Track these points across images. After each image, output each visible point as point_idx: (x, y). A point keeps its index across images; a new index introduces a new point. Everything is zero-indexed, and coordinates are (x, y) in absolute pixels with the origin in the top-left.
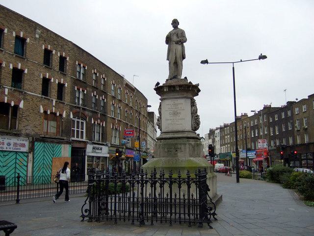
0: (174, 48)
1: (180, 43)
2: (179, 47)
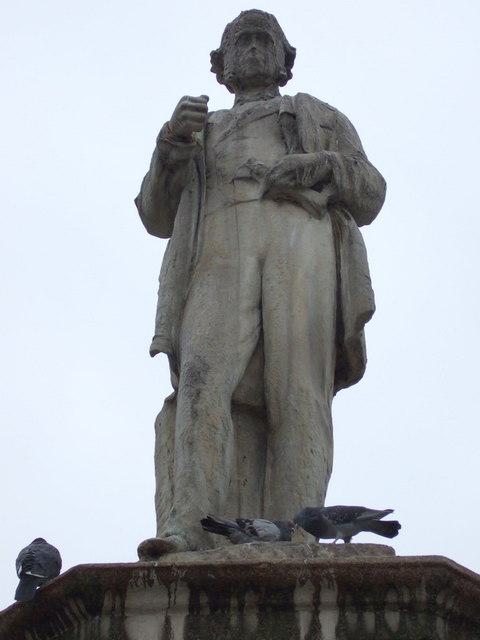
1: (319, 198)
2: (307, 236)
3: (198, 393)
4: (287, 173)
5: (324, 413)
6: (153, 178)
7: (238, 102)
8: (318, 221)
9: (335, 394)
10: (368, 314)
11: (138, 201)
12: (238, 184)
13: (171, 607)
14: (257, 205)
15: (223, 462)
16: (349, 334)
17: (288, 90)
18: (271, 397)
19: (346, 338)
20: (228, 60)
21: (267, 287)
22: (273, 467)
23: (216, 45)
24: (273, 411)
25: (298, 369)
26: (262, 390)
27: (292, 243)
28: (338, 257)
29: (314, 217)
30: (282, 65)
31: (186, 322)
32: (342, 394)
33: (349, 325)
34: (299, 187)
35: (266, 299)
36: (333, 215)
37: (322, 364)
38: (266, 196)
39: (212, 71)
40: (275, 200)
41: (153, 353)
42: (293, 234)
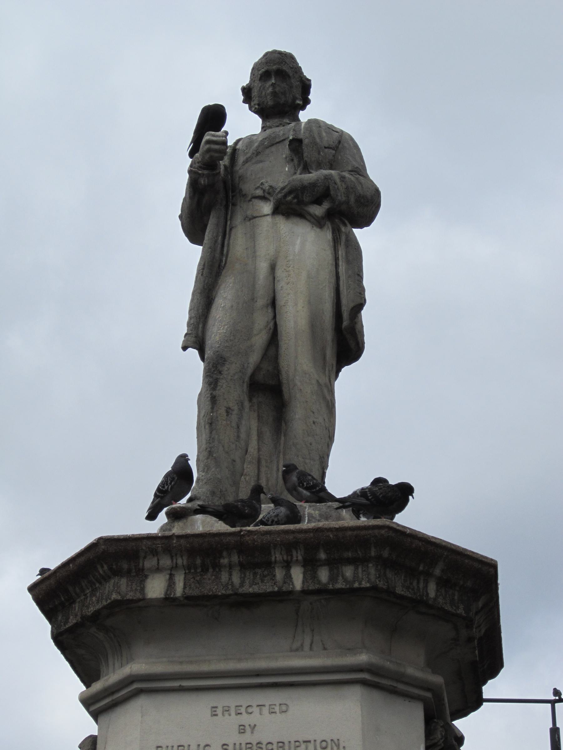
0: (265, 248)
1: (318, 210)
2: (303, 245)
4: (290, 192)
5: (325, 391)
6: (188, 200)
7: (264, 128)
8: (318, 230)
9: (337, 376)
10: (360, 306)
11: (181, 217)
13: (174, 568)
14: (269, 219)
15: (238, 437)
16: (345, 323)
17: (304, 116)
18: (284, 376)
19: (343, 326)
20: (255, 93)
21: (278, 286)
22: (285, 435)
23: (246, 81)
24: (285, 389)
25: (299, 360)
26: (277, 373)
28: (336, 259)
29: (316, 225)
30: (298, 96)
31: (211, 322)
32: (346, 370)
33: (346, 315)
34: (301, 202)
36: (333, 223)
37: (323, 350)
38: (276, 211)
40: (283, 214)
41: (185, 348)
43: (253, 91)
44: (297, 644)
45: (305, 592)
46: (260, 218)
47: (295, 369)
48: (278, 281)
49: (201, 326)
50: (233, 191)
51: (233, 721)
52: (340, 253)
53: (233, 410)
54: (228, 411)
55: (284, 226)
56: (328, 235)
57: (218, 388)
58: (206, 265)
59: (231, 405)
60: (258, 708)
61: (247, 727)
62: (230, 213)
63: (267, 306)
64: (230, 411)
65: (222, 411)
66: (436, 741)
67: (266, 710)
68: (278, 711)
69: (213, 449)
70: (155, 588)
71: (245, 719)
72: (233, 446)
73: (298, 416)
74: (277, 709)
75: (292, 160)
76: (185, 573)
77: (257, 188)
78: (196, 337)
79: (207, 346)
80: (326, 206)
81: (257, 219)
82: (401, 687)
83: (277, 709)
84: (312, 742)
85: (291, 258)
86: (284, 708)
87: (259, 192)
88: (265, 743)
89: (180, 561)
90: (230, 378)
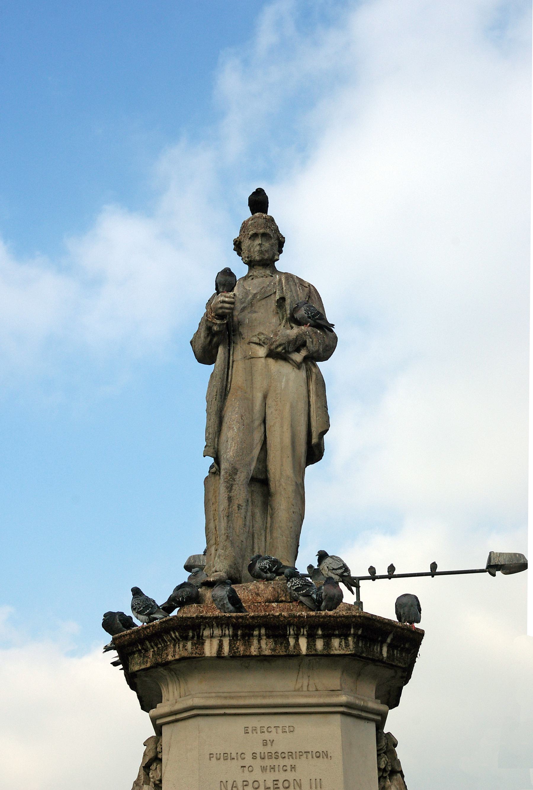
0: (260, 384)
2: (288, 377)
3: (232, 485)
5: (300, 488)
12: (253, 345)
13: (224, 636)
14: (263, 360)
15: (245, 525)
16: (314, 440)
21: (268, 412)
27: (283, 387)
28: (308, 391)
35: (268, 418)
36: (306, 364)
39: (234, 250)
42: (284, 380)
43: (242, 245)
44: (299, 686)
45: (307, 655)
46: (256, 359)
47: (281, 474)
48: (269, 407)
49: (216, 440)
50: (234, 331)
51: (259, 737)
52: (311, 387)
53: (242, 506)
54: (239, 506)
55: (274, 365)
56: (303, 374)
57: (233, 491)
58: (218, 391)
59: (240, 503)
60: (275, 728)
61: (268, 741)
62: (232, 350)
63: (260, 425)
64: (240, 507)
65: (235, 507)
66: (382, 747)
67: (280, 730)
68: (288, 732)
69: (229, 535)
70: (210, 649)
71: (267, 736)
72: (242, 531)
73: (282, 504)
74: (287, 730)
75: (278, 313)
76: (230, 640)
77: (253, 336)
78: (214, 449)
79: (222, 458)
80: (304, 353)
81: (253, 359)
82: (364, 714)
83: (287, 730)
84: (310, 753)
85: (279, 392)
86: (292, 729)
87: (255, 339)
88: (280, 753)
89: (227, 632)
90: (240, 483)
